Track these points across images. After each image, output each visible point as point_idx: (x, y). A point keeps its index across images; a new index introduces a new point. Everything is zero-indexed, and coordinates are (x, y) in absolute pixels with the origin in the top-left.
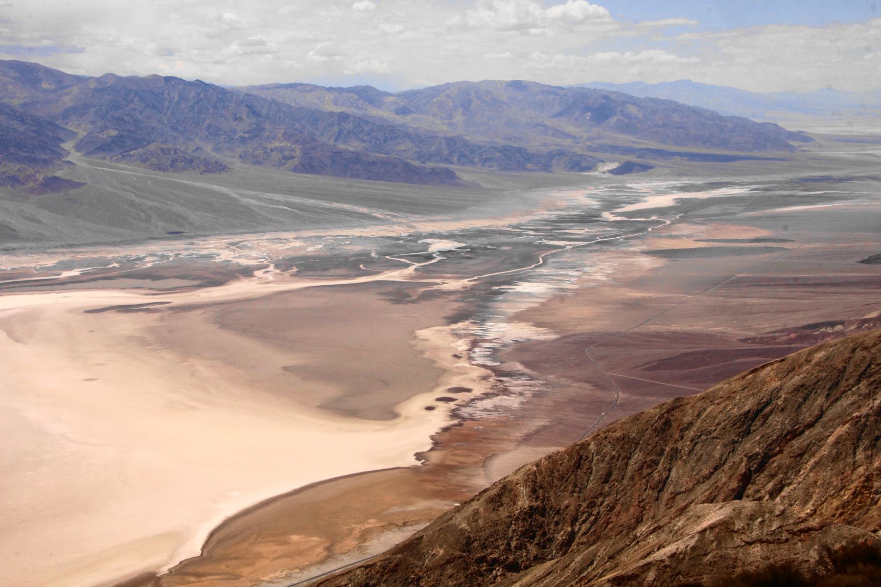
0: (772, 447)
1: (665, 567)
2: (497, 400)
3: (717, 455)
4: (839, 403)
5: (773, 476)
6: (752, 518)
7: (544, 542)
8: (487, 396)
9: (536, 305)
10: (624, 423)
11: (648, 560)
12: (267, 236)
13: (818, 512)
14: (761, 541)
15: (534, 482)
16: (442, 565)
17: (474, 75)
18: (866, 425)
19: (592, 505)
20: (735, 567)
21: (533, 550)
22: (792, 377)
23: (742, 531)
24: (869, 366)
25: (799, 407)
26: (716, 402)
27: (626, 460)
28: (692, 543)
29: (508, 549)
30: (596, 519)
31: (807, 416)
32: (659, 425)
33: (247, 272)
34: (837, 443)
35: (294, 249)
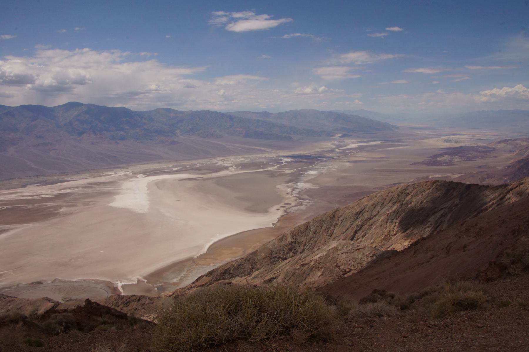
0: (364, 223)
1: (317, 261)
2: (298, 207)
3: (348, 225)
4: (384, 209)
5: (363, 231)
6: (344, 246)
7: (295, 252)
8: (296, 206)
9: (314, 178)
10: (321, 216)
11: (313, 259)
12: (233, 157)
13: (375, 242)
14: (346, 253)
15: (293, 234)
16: (263, 259)
17: (299, 107)
18: (390, 216)
19: (310, 241)
20: (337, 260)
21: (291, 254)
22: (371, 202)
23: (340, 250)
24: (393, 198)
25: (373, 210)
26: (349, 209)
27: (321, 227)
28: (326, 253)
29: (284, 254)
30: (311, 245)
31: (374, 214)
32: (331, 216)
33: (226, 168)
34: (382, 221)
35: (242, 161)
